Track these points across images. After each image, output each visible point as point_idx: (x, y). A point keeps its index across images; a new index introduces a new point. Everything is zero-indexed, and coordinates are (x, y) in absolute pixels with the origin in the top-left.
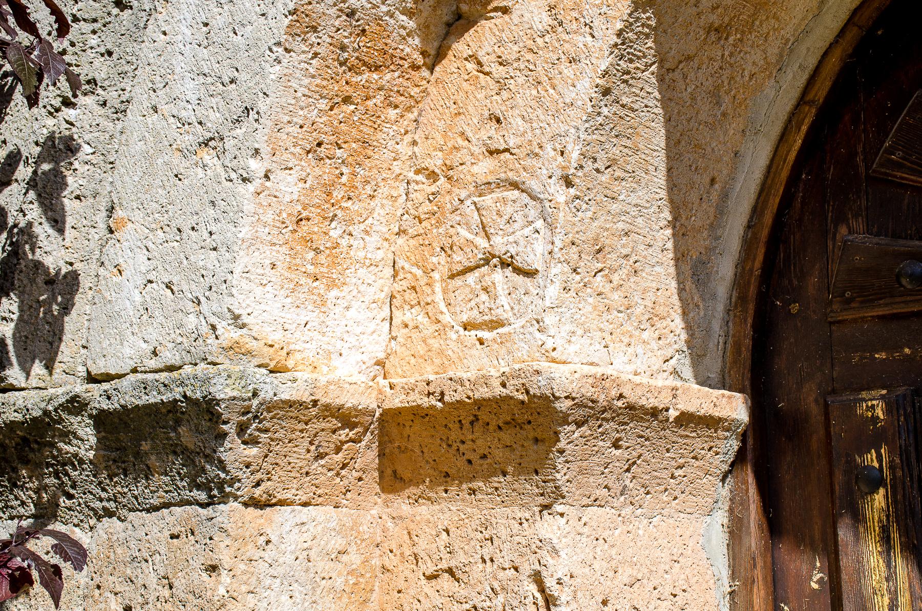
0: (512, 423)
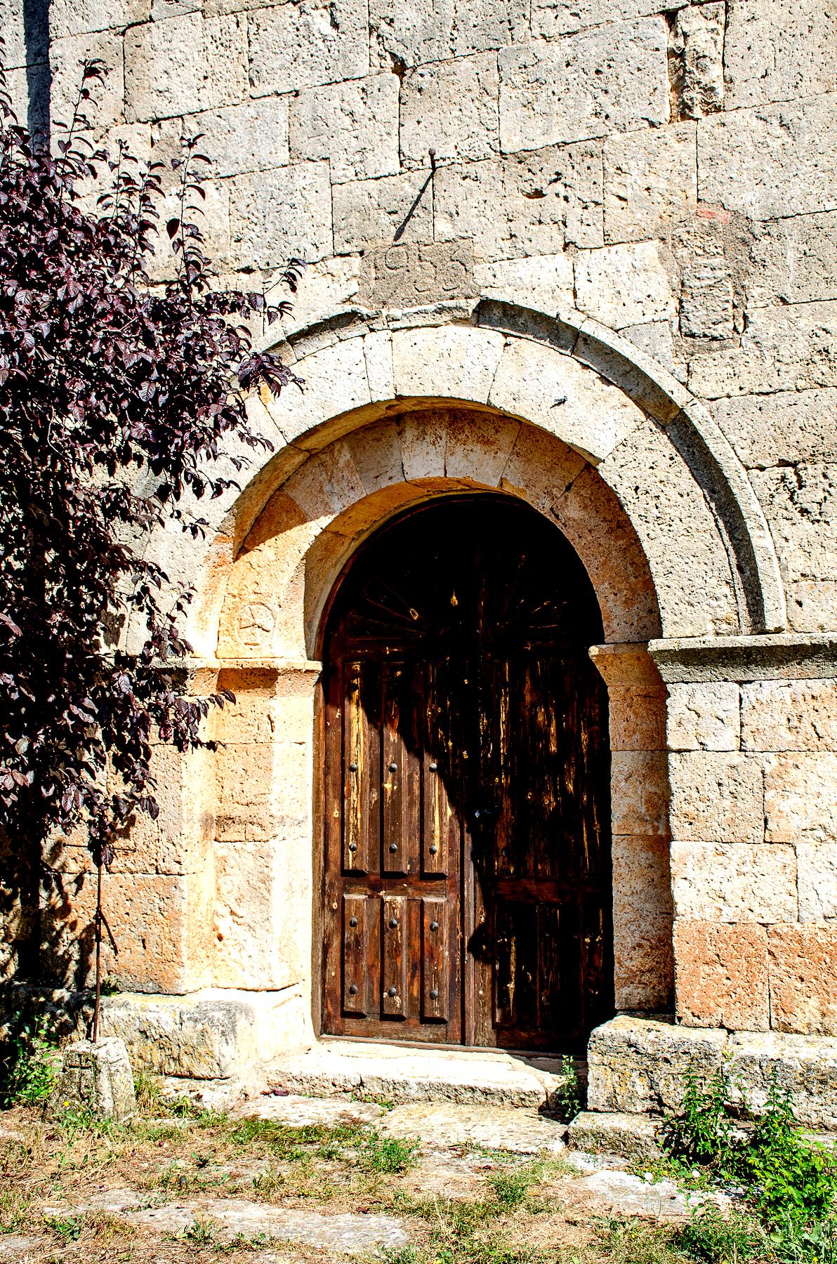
0: (264, 675)
